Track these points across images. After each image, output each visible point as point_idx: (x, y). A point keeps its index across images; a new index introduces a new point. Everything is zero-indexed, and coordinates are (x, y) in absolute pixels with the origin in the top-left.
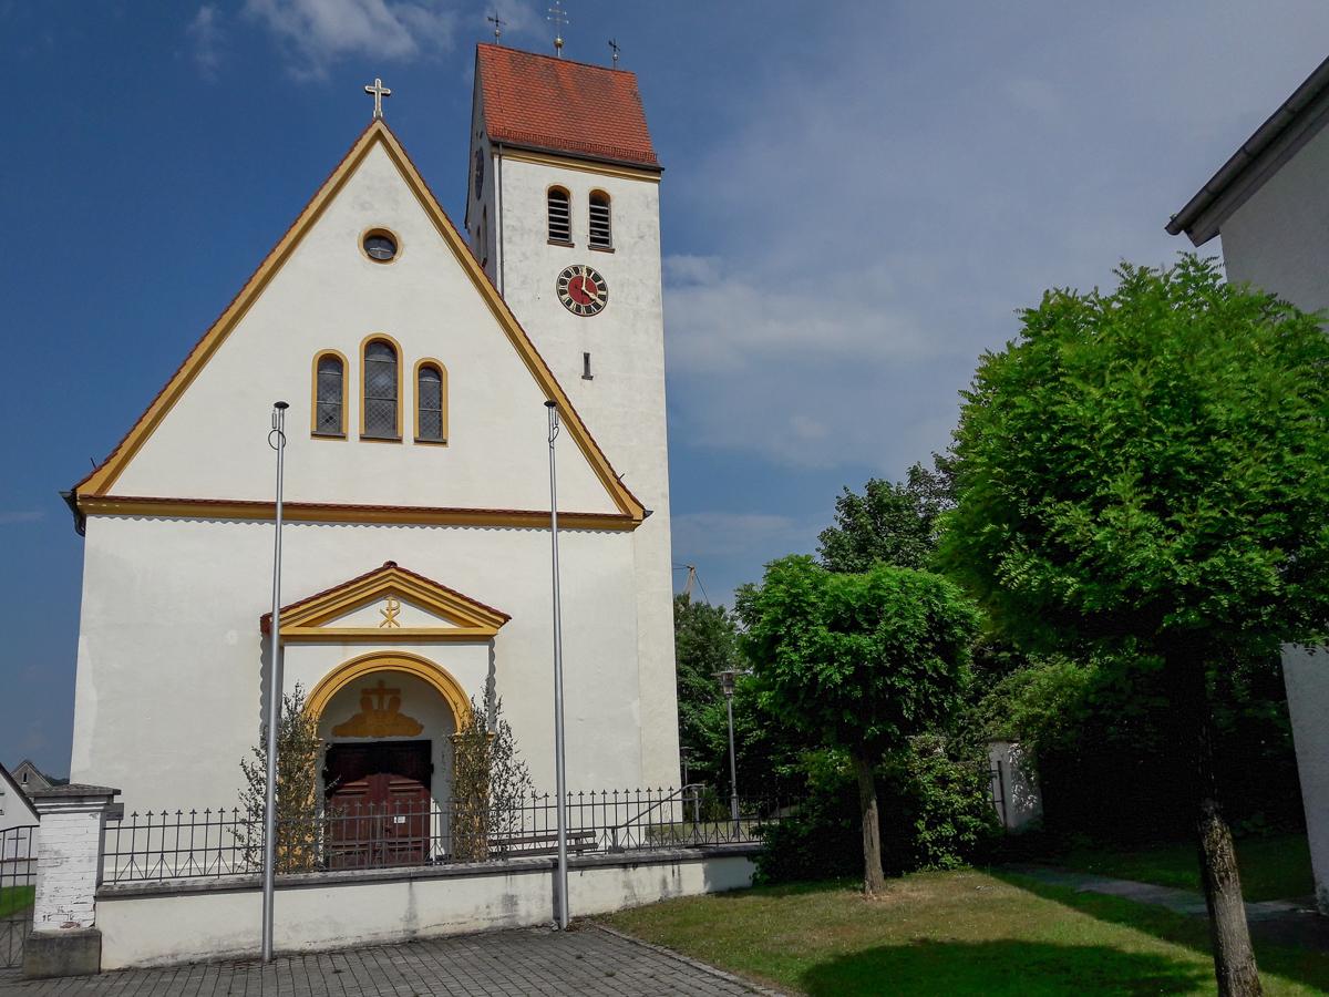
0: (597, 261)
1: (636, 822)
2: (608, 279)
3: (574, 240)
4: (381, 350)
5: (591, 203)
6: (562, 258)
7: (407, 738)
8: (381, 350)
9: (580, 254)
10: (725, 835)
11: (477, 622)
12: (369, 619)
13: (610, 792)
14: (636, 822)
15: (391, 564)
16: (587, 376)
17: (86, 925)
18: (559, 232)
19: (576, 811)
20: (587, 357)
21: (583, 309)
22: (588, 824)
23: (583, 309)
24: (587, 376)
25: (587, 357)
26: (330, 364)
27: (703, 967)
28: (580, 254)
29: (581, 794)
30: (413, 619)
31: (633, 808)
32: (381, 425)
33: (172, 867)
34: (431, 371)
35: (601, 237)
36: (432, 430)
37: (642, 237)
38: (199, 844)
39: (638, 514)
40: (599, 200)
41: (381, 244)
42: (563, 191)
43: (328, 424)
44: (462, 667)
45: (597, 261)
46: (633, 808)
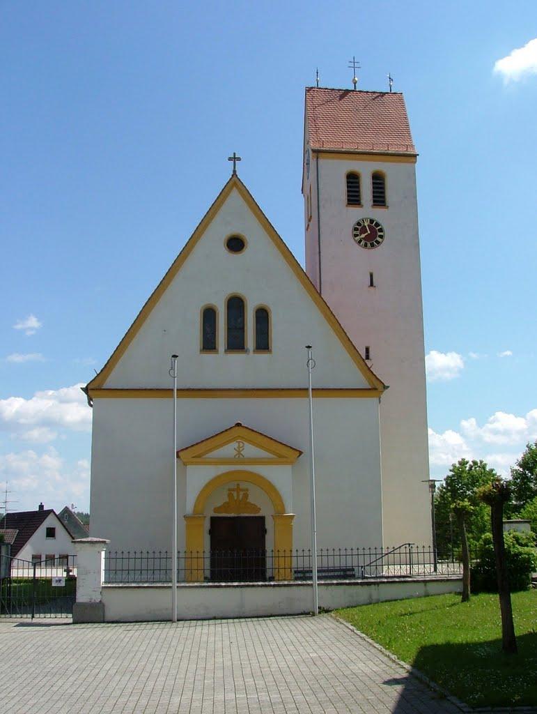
0: (378, 214)
1: (374, 564)
2: (384, 225)
3: (363, 202)
4: (236, 305)
5: (373, 179)
6: (357, 214)
7: (252, 515)
8: (236, 305)
9: (366, 211)
10: (393, 571)
11: (288, 452)
12: (229, 450)
13: (337, 549)
14: (374, 564)
15: (238, 425)
16: (372, 285)
17: (98, 601)
18: (354, 198)
19: (282, 560)
20: (371, 276)
21: (369, 245)
22: (349, 564)
23: (369, 245)
24: (372, 285)
25: (371, 276)
26: (209, 315)
27: (256, 583)
28: (366, 211)
29: (358, 549)
30: (250, 450)
31: (367, 558)
32: (236, 344)
33: (133, 577)
34: (263, 316)
35: (379, 199)
36: (263, 344)
37: (406, 197)
38: (144, 567)
39: (380, 387)
40: (378, 180)
41: (236, 244)
42: (356, 175)
43: (209, 344)
44: (279, 476)
45: (378, 214)
46: (367, 558)
